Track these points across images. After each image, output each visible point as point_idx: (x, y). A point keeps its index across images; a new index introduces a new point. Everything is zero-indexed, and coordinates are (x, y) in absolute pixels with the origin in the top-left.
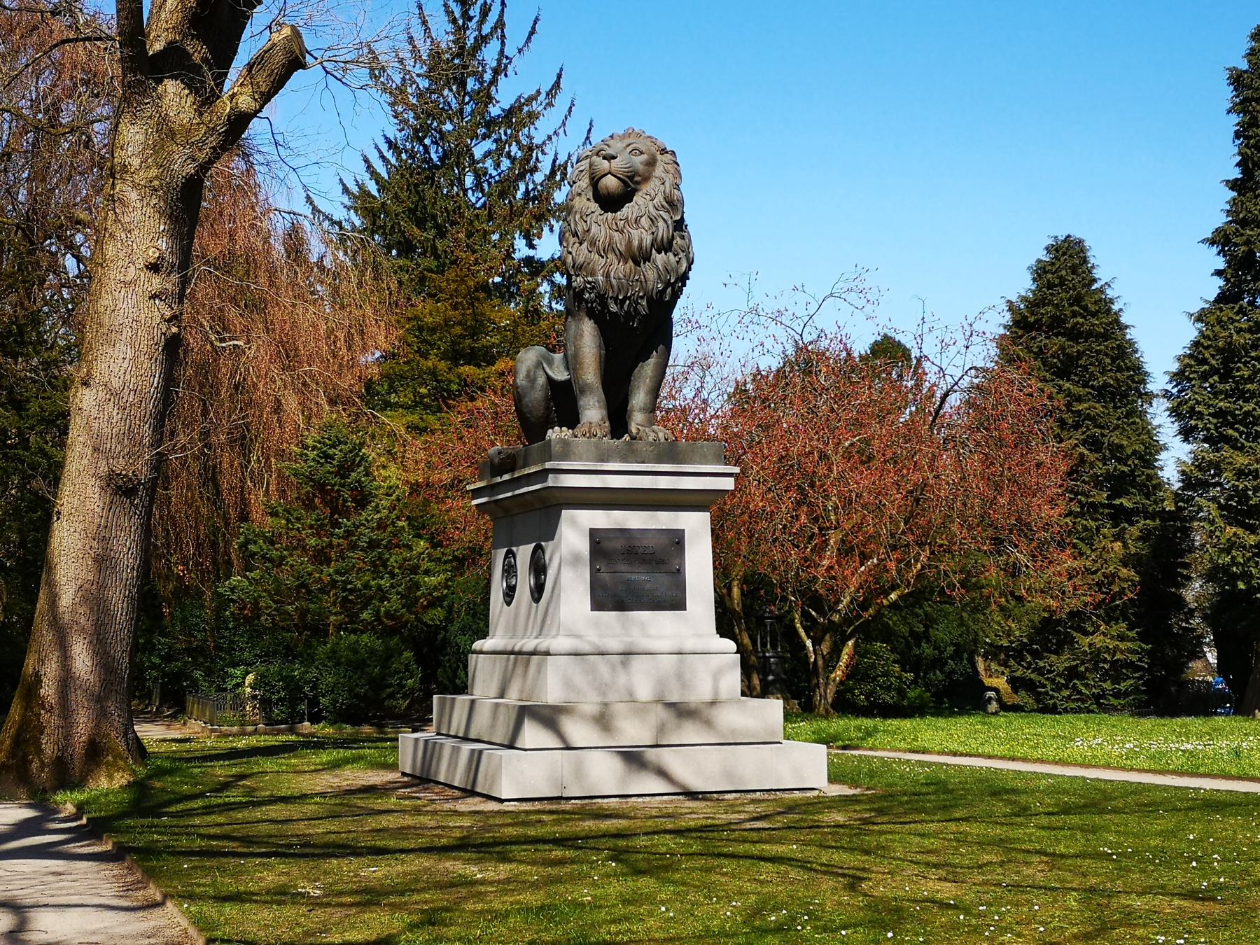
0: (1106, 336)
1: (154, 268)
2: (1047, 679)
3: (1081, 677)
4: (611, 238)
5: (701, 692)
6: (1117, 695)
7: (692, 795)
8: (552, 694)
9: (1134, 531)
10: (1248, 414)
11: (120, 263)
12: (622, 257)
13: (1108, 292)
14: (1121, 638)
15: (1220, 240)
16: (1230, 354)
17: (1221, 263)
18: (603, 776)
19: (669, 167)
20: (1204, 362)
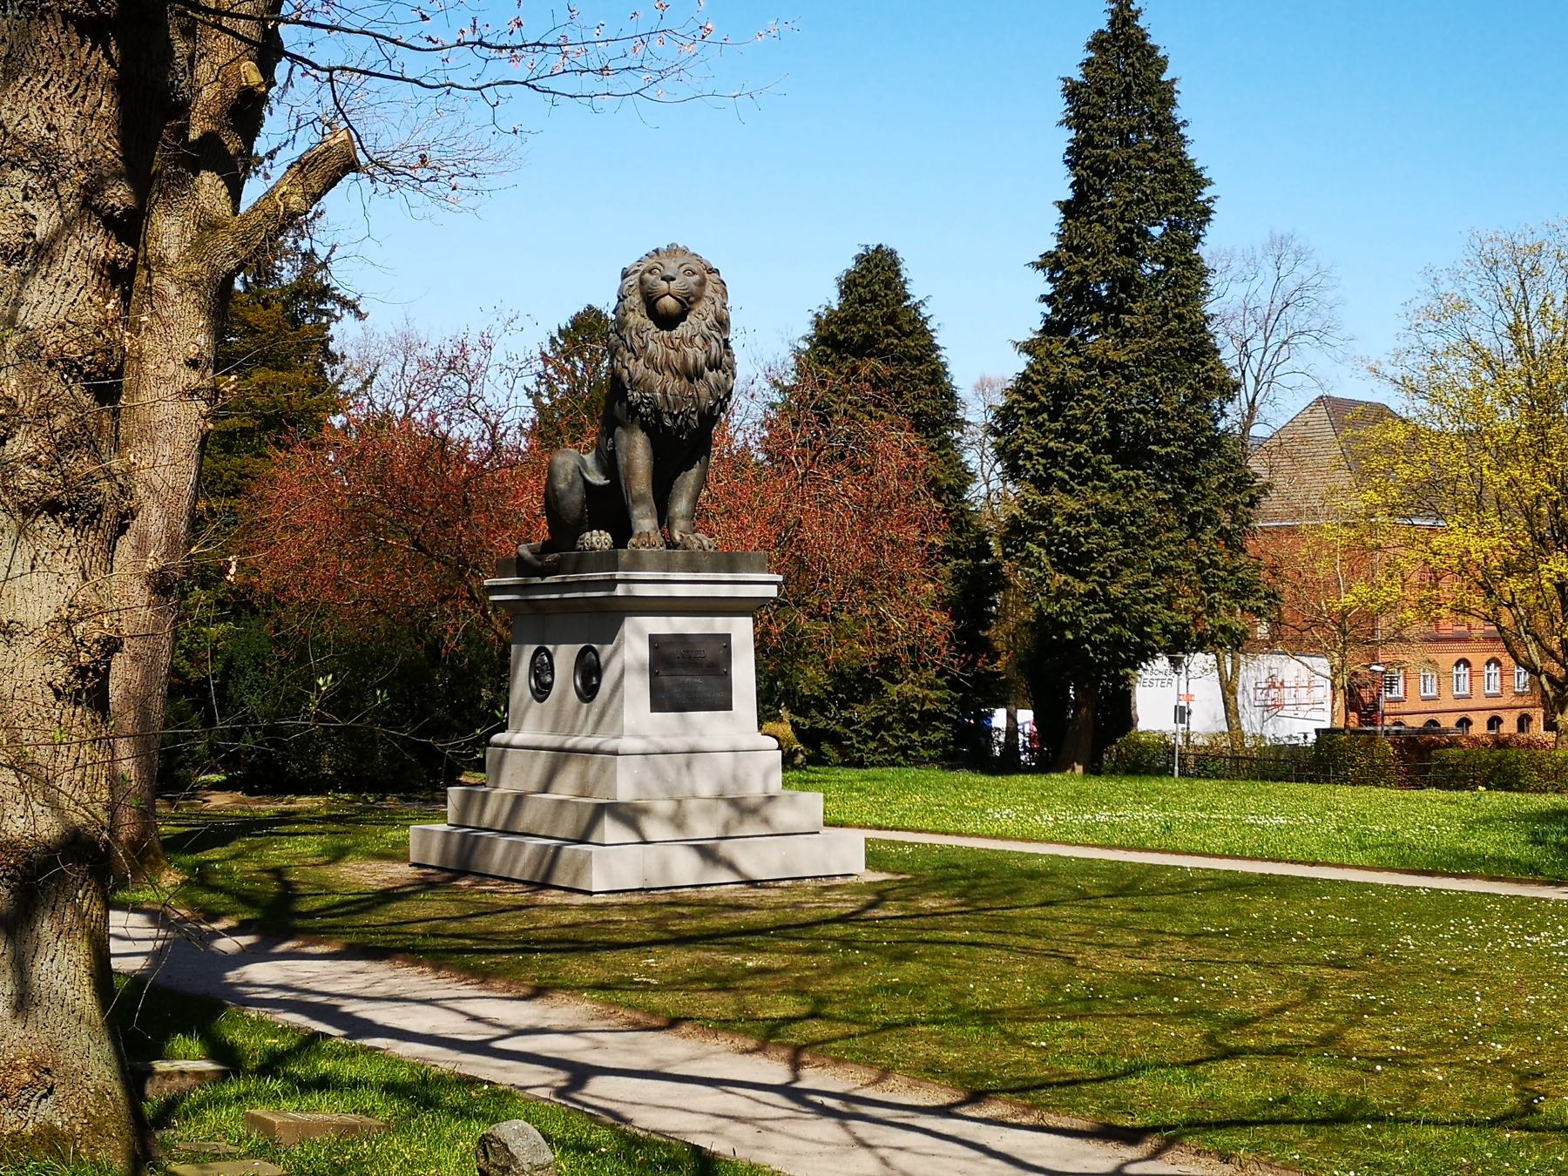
0: (919, 360)
1: (193, 364)
2: (853, 731)
3: (889, 728)
4: (668, 355)
5: (754, 791)
6: (929, 745)
7: (752, 883)
8: (625, 791)
9: (945, 571)
10: (1079, 455)
11: (158, 359)
12: (677, 373)
13: (922, 310)
14: (931, 686)
15: (1050, 263)
16: (1062, 392)
17: (1048, 289)
18: (685, 869)
19: (717, 287)
20: (1033, 398)
